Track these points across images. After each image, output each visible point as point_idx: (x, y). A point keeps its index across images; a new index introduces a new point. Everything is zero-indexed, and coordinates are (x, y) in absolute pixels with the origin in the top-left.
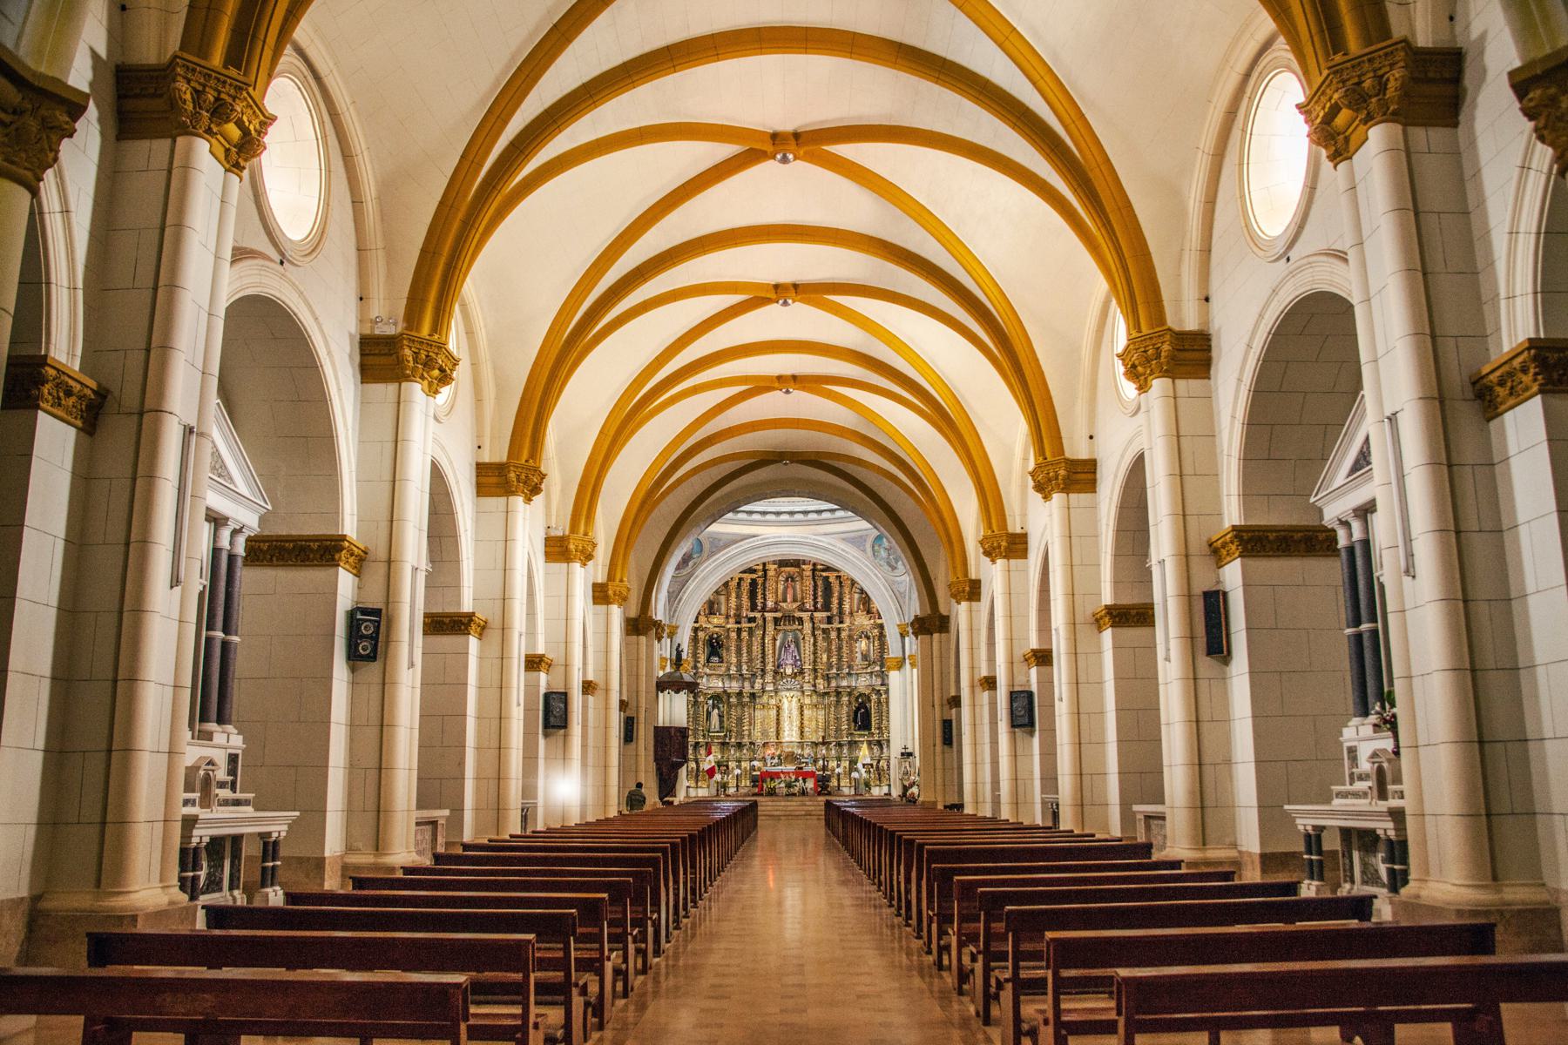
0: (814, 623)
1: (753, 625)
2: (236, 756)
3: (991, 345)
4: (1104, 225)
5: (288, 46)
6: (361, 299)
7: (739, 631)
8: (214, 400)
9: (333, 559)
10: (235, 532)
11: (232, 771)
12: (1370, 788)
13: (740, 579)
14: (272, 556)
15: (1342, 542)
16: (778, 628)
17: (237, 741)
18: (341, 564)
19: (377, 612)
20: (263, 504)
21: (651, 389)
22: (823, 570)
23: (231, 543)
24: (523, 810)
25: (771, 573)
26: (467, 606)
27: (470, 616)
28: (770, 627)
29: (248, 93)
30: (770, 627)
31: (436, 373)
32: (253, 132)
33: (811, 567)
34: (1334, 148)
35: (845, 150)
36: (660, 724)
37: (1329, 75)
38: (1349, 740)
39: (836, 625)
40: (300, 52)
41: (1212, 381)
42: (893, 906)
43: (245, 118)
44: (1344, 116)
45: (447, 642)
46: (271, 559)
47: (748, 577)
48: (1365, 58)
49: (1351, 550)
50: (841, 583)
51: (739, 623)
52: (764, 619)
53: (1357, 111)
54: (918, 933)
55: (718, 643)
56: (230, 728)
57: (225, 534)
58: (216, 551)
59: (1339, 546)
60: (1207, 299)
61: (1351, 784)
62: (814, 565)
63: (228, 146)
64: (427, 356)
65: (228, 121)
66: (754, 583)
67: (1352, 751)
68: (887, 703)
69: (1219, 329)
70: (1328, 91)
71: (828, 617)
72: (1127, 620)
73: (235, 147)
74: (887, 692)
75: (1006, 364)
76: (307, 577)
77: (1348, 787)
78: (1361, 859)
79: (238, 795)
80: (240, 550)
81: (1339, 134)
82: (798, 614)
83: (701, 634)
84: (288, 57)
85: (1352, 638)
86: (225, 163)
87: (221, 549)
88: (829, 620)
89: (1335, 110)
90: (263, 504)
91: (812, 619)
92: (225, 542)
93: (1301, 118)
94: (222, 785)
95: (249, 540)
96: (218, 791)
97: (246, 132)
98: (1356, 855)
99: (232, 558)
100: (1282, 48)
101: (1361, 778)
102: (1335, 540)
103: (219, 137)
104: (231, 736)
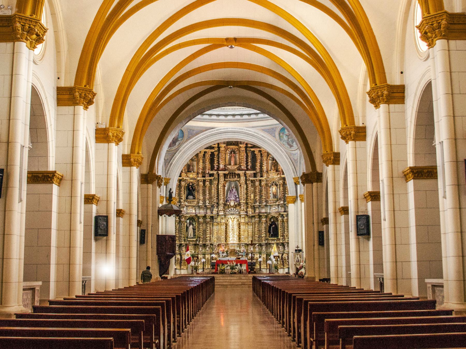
0: (246, 177)
1: (212, 178)
7: (204, 181)
13: (205, 152)
16: (226, 179)
22: (251, 147)
24: (83, 282)
25: (222, 149)
26: (52, 168)
28: (222, 179)
30: (222, 179)
31: (34, 36)
33: (245, 146)
45: (40, 187)
47: (209, 151)
50: (261, 154)
52: (219, 175)
55: (192, 188)
74: (287, 215)
82: (237, 172)
88: (255, 175)
91: (245, 175)
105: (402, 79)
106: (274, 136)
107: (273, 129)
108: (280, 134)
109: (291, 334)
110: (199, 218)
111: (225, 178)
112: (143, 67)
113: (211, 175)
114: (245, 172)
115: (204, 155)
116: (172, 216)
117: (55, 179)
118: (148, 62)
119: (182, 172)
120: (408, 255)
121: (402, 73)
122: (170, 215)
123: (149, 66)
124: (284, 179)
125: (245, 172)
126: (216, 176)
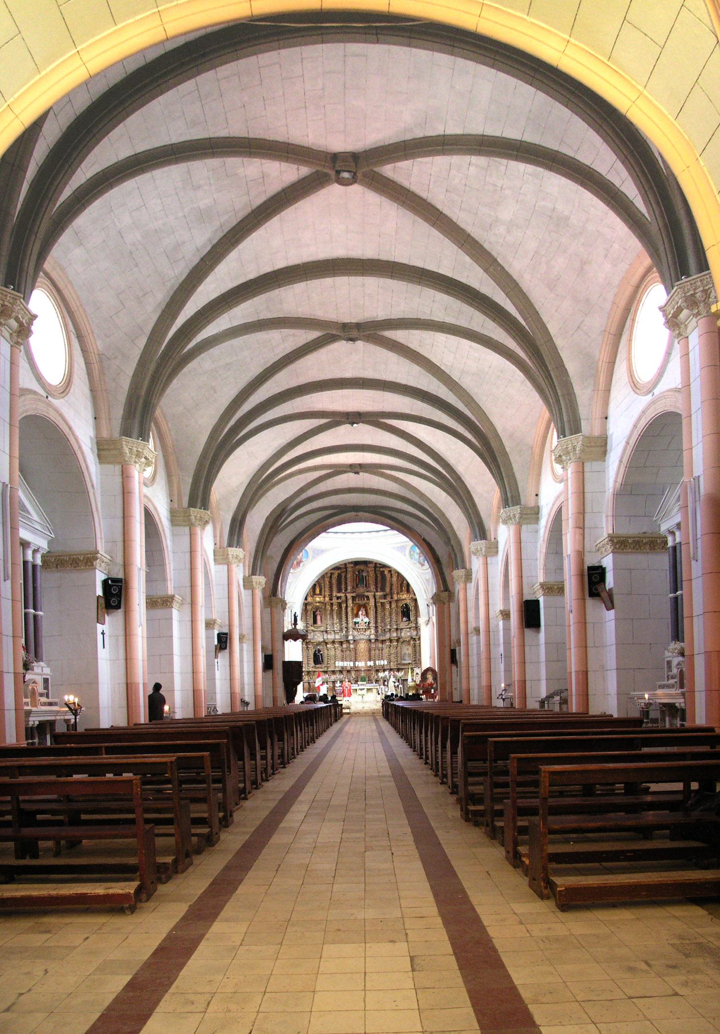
0: (375, 599)
1: (340, 601)
2: (47, 679)
3: (473, 440)
4: (546, 377)
5: (41, 273)
6: (95, 418)
7: (332, 604)
8: (17, 473)
9: (92, 565)
10: (35, 552)
11: (46, 687)
12: (676, 682)
13: (332, 574)
14: (57, 565)
15: (670, 544)
16: (355, 602)
17: (47, 671)
18: (97, 567)
19: (226, 634)
20: (49, 534)
21: (277, 468)
22: (381, 567)
23: (33, 558)
24: (208, 709)
25: (349, 569)
26: (171, 592)
27: (172, 597)
28: (350, 602)
29: (20, 302)
30: (350, 602)
31: (143, 460)
32: (25, 324)
33: (374, 565)
34: (678, 332)
35: (399, 336)
36: (287, 659)
37: (677, 289)
38: (668, 657)
39: (389, 599)
40: (48, 276)
41: (606, 463)
42: (422, 758)
43: (20, 316)
44: (685, 312)
45: (159, 613)
46: (57, 567)
47: (336, 573)
48: (698, 280)
49: (674, 548)
50: (391, 575)
51: (332, 600)
52: (346, 597)
53: (692, 310)
54: (436, 773)
56: (42, 664)
57: (29, 553)
58: (25, 563)
59: (668, 546)
60: (606, 418)
61: (668, 680)
62: (376, 564)
63: (11, 332)
64: (137, 451)
65: (10, 317)
66: (339, 576)
67: (669, 663)
68: (420, 646)
69: (612, 434)
70: (676, 299)
71: (384, 595)
72: (553, 591)
73: (15, 332)
74: (419, 639)
75: (486, 455)
76: (74, 577)
77: (666, 682)
78: (670, 721)
79: (50, 700)
80: (39, 562)
81: (681, 324)
82: (366, 594)
83: (309, 608)
84: (41, 279)
85: (672, 600)
86: (10, 342)
87: (37, 565)
88: (385, 597)
89: (680, 310)
90: (49, 534)
91: (374, 596)
92: (30, 558)
93: (661, 313)
94: (41, 695)
95: (43, 556)
96: (40, 698)
97: (21, 324)
98: (667, 719)
99: (34, 567)
100: (655, 275)
101: (673, 678)
102: (666, 543)
103: (6, 327)
104: (44, 669)
105: (537, 501)
106: (405, 555)
107: (403, 546)
108: (410, 552)
109: (428, 761)
110: (326, 643)
111: (353, 600)
112: (261, 492)
113: (338, 598)
114: (375, 594)
115: (331, 577)
116: (298, 641)
117: (175, 603)
118: (265, 488)
119: (307, 595)
120: (538, 655)
121: (537, 495)
122: (295, 640)
123: (268, 490)
124: (416, 600)
125: (375, 594)
126: (344, 598)
